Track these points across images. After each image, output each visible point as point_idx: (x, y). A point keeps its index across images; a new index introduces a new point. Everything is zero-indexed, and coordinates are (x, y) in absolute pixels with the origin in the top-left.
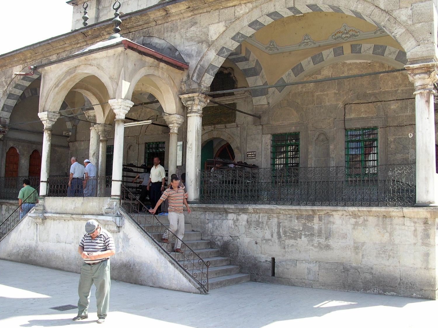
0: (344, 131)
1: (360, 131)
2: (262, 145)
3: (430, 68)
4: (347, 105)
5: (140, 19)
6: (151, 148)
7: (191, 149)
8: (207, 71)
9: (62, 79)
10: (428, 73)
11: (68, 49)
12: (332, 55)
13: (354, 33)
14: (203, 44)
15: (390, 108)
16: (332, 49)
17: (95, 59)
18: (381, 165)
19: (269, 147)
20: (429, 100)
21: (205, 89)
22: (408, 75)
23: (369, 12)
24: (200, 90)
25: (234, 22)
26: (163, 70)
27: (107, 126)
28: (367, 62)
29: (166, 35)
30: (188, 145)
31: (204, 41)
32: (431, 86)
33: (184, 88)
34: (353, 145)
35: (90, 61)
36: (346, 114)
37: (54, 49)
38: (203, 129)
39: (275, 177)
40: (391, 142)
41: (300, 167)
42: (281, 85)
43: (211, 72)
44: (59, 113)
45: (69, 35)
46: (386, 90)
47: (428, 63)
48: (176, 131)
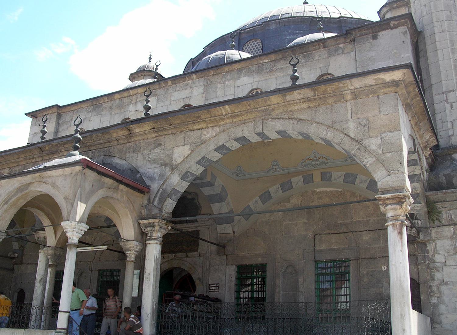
0: (314, 263)
1: (331, 263)
2: (226, 277)
3: (401, 198)
4: (317, 235)
5: (101, 137)
6: (105, 276)
7: (148, 280)
8: (170, 196)
9: (13, 196)
10: (400, 203)
11: (22, 163)
12: (301, 183)
13: (324, 160)
14: (167, 167)
15: (362, 239)
16: (301, 177)
18: (353, 301)
19: (234, 279)
20: (402, 232)
21: (166, 215)
22: (380, 205)
23: (339, 141)
24: (161, 216)
25: (199, 145)
26: (122, 193)
27: (58, 249)
28: (337, 191)
29: (127, 155)
30: (146, 275)
31: (168, 164)
32: (403, 217)
33: (144, 212)
34: (324, 278)
35: (45, 179)
36: (316, 245)
37: (8, 162)
38: (163, 258)
39: (240, 312)
40: (364, 275)
41: (267, 302)
42: (248, 214)
43: (174, 197)
44: (5, 233)
45: (25, 149)
46: (358, 220)
47: (399, 194)
48: (133, 259)
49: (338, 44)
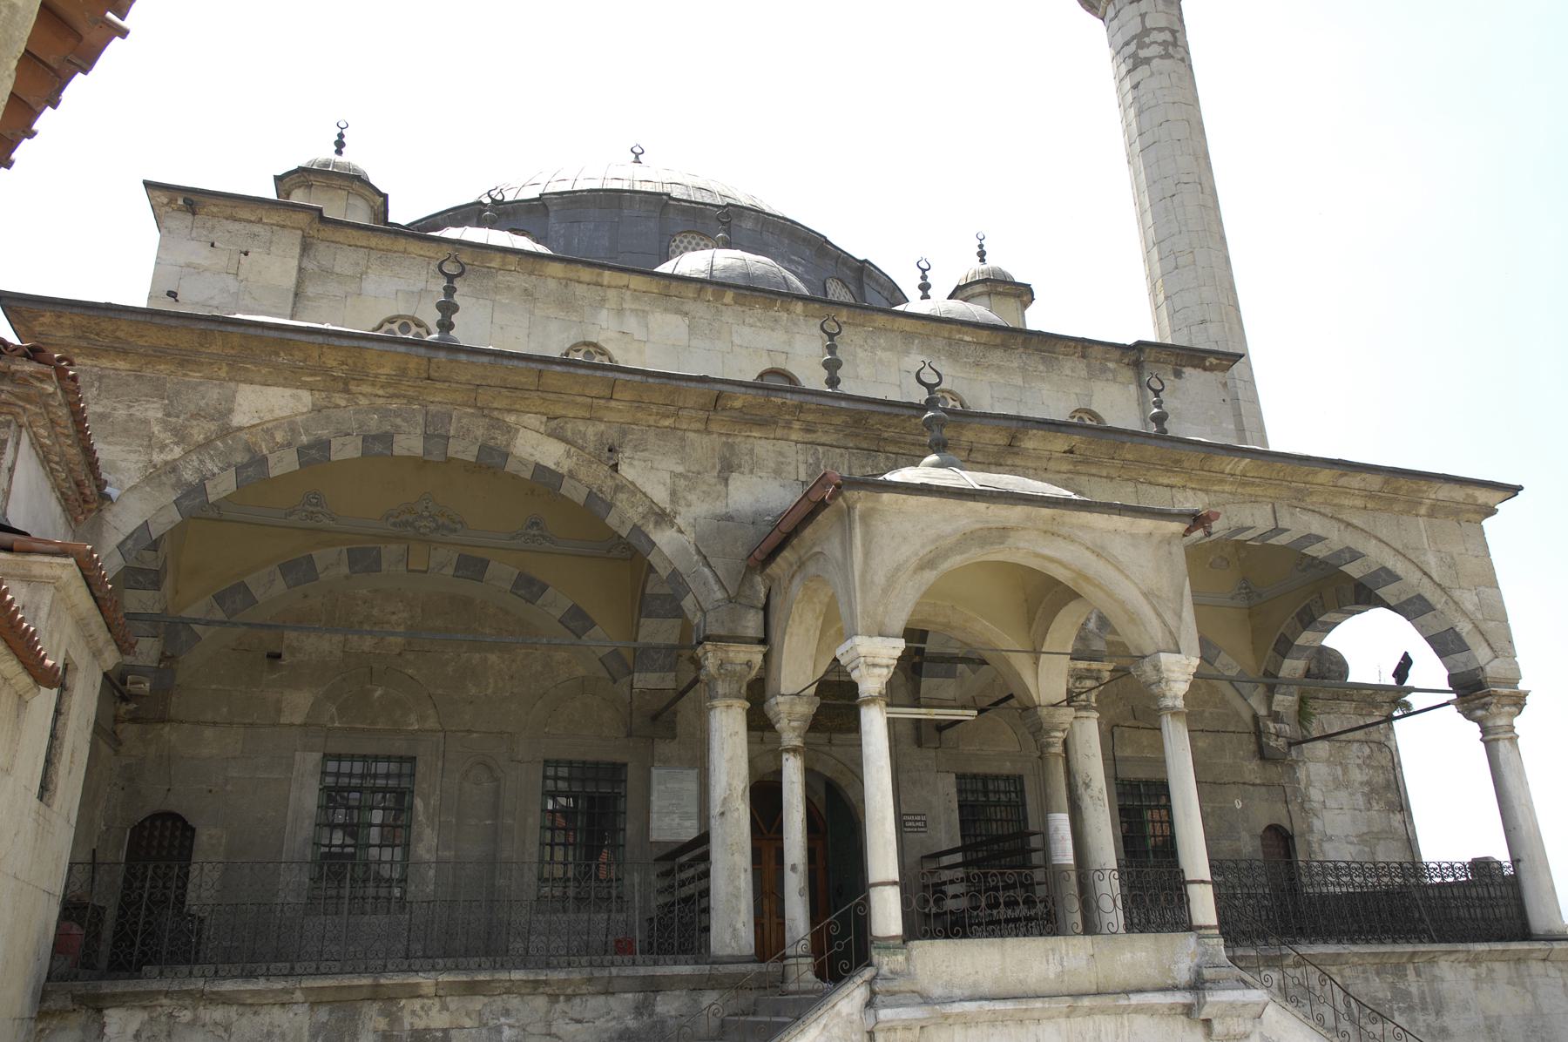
17: (1082, 527)
49: (1107, 360)
